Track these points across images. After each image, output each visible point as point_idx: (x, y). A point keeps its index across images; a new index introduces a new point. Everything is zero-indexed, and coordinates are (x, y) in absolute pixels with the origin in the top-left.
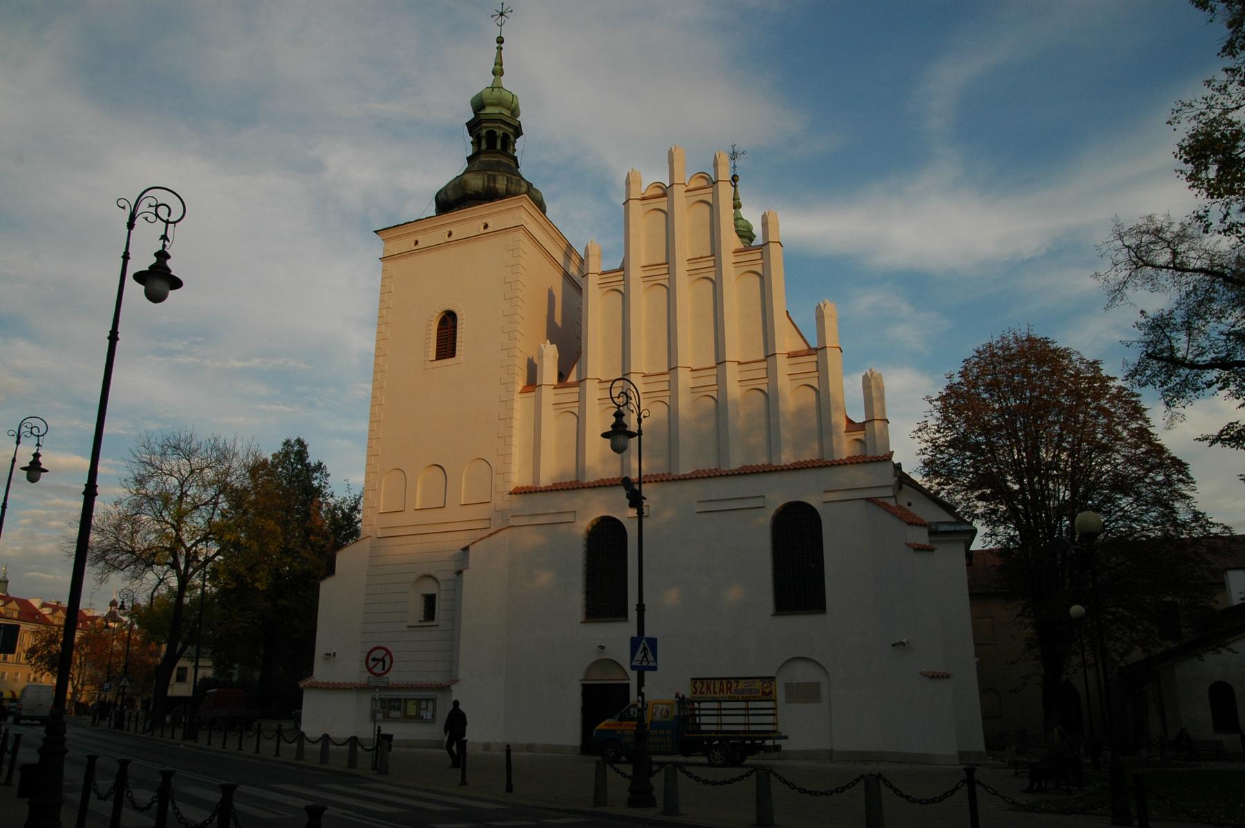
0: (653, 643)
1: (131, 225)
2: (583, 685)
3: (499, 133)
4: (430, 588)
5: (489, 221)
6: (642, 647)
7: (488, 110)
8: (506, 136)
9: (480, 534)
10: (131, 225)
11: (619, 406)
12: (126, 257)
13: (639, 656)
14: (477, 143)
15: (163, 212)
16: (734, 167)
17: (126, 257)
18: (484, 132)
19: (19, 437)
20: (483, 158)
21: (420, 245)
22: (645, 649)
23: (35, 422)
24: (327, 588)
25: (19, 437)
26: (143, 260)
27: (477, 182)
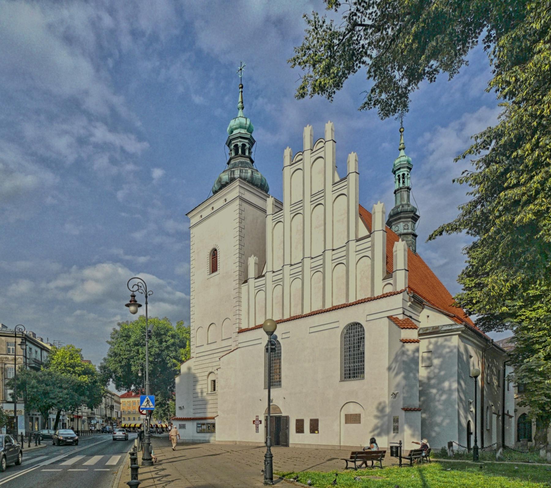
3: (240, 144)
6: (146, 400)
11: (133, 291)
18: (232, 147)
20: (232, 162)
21: (203, 217)
22: (148, 401)
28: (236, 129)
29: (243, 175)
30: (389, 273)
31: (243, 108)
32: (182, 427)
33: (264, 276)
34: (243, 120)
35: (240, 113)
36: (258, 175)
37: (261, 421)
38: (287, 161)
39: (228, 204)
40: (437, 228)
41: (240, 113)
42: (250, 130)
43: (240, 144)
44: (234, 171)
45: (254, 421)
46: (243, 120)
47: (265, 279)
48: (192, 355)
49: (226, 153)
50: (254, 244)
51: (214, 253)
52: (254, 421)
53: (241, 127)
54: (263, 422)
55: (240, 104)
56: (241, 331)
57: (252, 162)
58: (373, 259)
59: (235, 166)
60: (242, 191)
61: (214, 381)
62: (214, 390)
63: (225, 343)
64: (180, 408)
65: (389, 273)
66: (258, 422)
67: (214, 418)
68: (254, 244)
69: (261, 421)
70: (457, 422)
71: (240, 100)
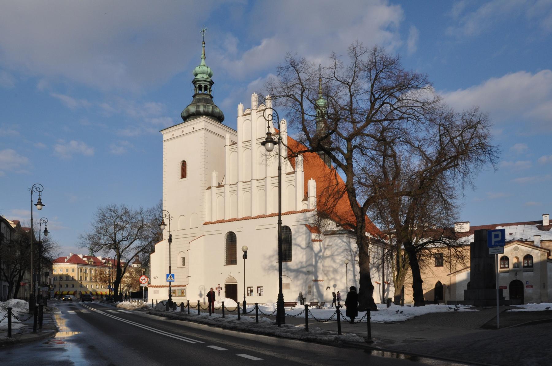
0: (173, 276)
1: (32, 194)
2: (226, 285)
3: (203, 85)
7: (199, 76)
8: (206, 86)
9: (191, 239)
10: (32, 194)
12: (32, 201)
13: (169, 278)
15: (38, 189)
17: (32, 201)
18: (197, 86)
19: (32, 192)
20: (197, 97)
21: (174, 136)
23: (38, 186)
25: (32, 192)
26: (36, 201)
27: (192, 109)
28: (200, 73)
29: (206, 110)
30: (306, 198)
31: (205, 58)
32: (157, 292)
33: (223, 186)
34: (205, 69)
35: (203, 62)
36: (217, 110)
37: (222, 288)
38: (240, 112)
39: (194, 131)
40: (263, 293)
41: (203, 62)
42: (210, 75)
43: (203, 85)
44: (199, 105)
46: (205, 69)
47: (225, 189)
49: (191, 90)
50: (216, 162)
51: (184, 164)
53: (203, 73)
54: (224, 289)
55: (203, 56)
56: (206, 223)
57: (212, 97)
58: (295, 187)
59: (199, 101)
60: (207, 124)
61: (184, 258)
62: (184, 264)
63: (193, 231)
64: (155, 278)
65: (306, 198)
66: (219, 289)
67: (185, 286)
68: (216, 162)
69: (222, 288)
70: (391, 325)
71: (203, 53)
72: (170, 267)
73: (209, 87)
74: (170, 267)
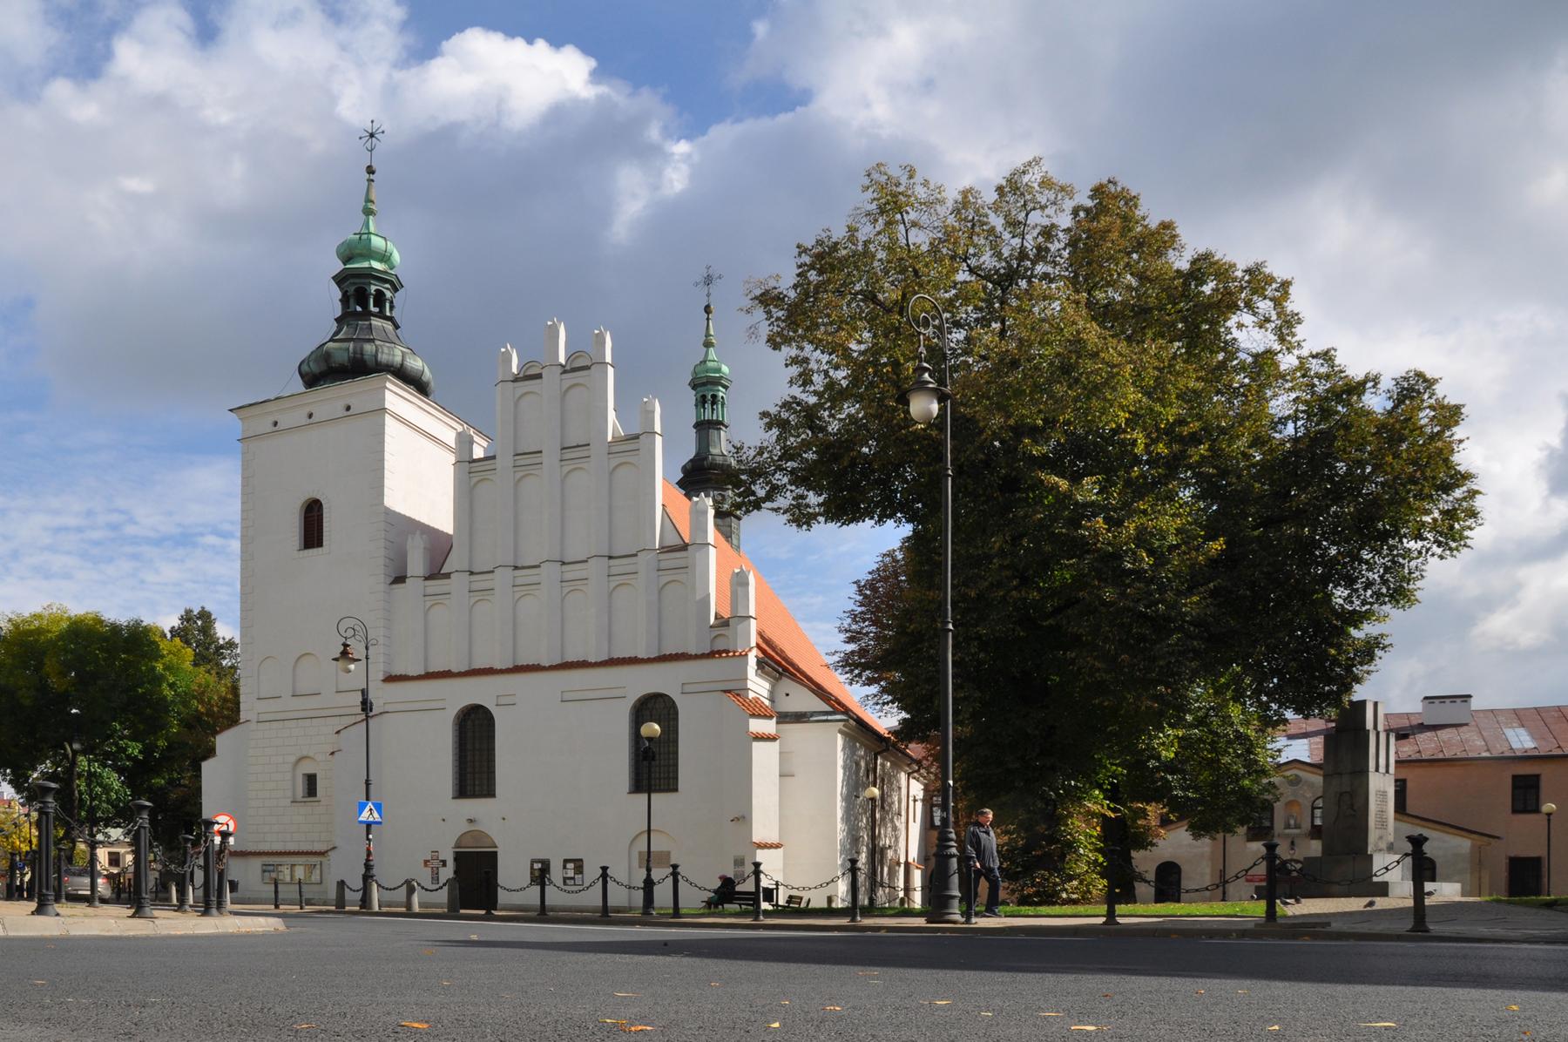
2: (457, 853)
4: (308, 768)
5: (352, 402)
14: (345, 300)
16: (708, 295)
18: (352, 290)
24: (206, 766)
27: (342, 352)
37: (444, 863)
45: (426, 862)
48: (243, 716)
52: (426, 862)
57: (397, 327)
69: (444, 863)
72: (368, 783)
73: (388, 294)
74: (368, 783)
